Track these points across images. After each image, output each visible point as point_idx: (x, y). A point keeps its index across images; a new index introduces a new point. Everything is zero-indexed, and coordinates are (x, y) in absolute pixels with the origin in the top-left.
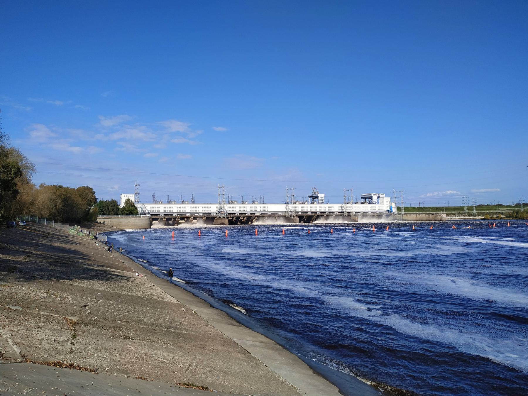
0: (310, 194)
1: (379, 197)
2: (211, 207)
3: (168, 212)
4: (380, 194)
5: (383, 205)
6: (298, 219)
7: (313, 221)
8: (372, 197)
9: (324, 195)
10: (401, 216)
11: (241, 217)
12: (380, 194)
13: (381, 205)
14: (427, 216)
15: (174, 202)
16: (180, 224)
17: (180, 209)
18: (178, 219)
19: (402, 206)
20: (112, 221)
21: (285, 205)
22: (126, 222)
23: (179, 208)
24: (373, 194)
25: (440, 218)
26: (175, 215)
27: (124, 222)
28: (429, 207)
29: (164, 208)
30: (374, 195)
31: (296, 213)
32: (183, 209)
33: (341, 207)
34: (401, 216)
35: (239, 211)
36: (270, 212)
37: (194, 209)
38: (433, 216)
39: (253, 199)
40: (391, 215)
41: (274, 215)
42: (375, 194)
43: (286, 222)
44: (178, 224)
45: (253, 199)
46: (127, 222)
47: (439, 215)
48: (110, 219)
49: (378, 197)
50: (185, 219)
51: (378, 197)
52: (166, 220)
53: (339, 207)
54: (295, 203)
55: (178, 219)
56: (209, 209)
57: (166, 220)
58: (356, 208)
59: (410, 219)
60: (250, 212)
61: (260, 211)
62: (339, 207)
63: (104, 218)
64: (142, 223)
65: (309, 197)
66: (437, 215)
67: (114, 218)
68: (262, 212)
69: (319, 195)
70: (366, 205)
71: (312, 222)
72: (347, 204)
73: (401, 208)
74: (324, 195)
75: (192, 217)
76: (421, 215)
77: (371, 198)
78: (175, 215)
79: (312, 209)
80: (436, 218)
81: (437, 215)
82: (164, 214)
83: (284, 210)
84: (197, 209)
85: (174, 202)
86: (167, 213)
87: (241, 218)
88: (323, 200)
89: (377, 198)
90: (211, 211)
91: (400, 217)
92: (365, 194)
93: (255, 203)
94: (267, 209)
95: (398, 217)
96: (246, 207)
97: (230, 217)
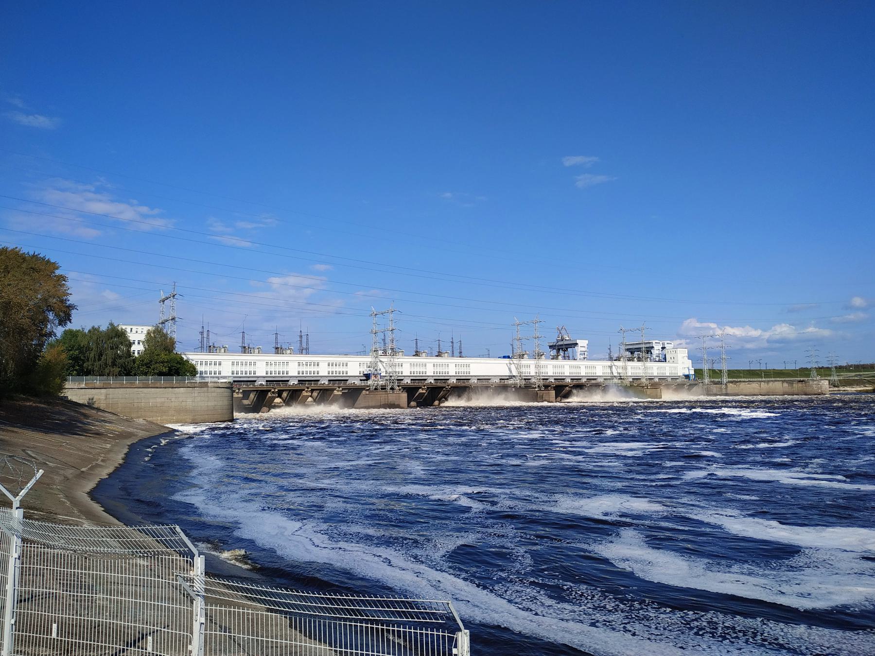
0: (553, 341)
1: (665, 348)
2: (471, 365)
3: (244, 375)
4: (666, 342)
5: (675, 365)
6: (554, 391)
7: (440, 401)
8: (653, 347)
9: (587, 342)
10: (724, 386)
11: (420, 388)
12: (666, 342)
13: (671, 365)
14: (785, 385)
15: (257, 351)
16: (275, 407)
17: (272, 369)
18: (273, 392)
19: (706, 367)
20: (111, 396)
21: (507, 361)
22: (158, 400)
23: (271, 364)
24: (654, 342)
25: (818, 389)
26: (407, 382)
27: (151, 401)
28: (736, 370)
29: (233, 364)
30: (656, 343)
31: (543, 379)
32: (281, 369)
33: (611, 367)
34: (724, 386)
35: (456, 373)
36: (475, 376)
37: (309, 369)
38: (800, 385)
39: (439, 345)
40: (696, 384)
41: (485, 385)
42: (669, 342)
43: (521, 401)
44: (271, 406)
45: (439, 345)
46: (163, 400)
47: (815, 383)
48: (103, 391)
49: (662, 348)
50: (285, 394)
51: (663, 348)
52: (240, 395)
53: (604, 367)
54: (521, 356)
55: (273, 392)
56: (344, 369)
57: (240, 395)
58: (634, 371)
59: (745, 392)
60: (300, 379)
61: (326, 374)
62: (604, 367)
63: (83, 386)
64: (210, 404)
65: (550, 347)
66: (811, 383)
67: (118, 386)
68: (460, 378)
69: (578, 341)
70: (560, 362)
71: (439, 404)
72: (616, 360)
73: (701, 370)
74: (587, 342)
75: (239, 389)
76: (771, 384)
77: (649, 350)
78: (407, 382)
79: (438, 369)
80: (809, 390)
81: (811, 383)
82: (411, 380)
83: (506, 373)
84: (316, 369)
85: (257, 351)
86: (240, 377)
87: (422, 392)
88: (586, 353)
89: (661, 349)
90: (320, 374)
91: (721, 388)
92: (633, 340)
93: (397, 354)
94: (424, 370)
95: (714, 388)
96: (255, 364)
97: (338, 389)
